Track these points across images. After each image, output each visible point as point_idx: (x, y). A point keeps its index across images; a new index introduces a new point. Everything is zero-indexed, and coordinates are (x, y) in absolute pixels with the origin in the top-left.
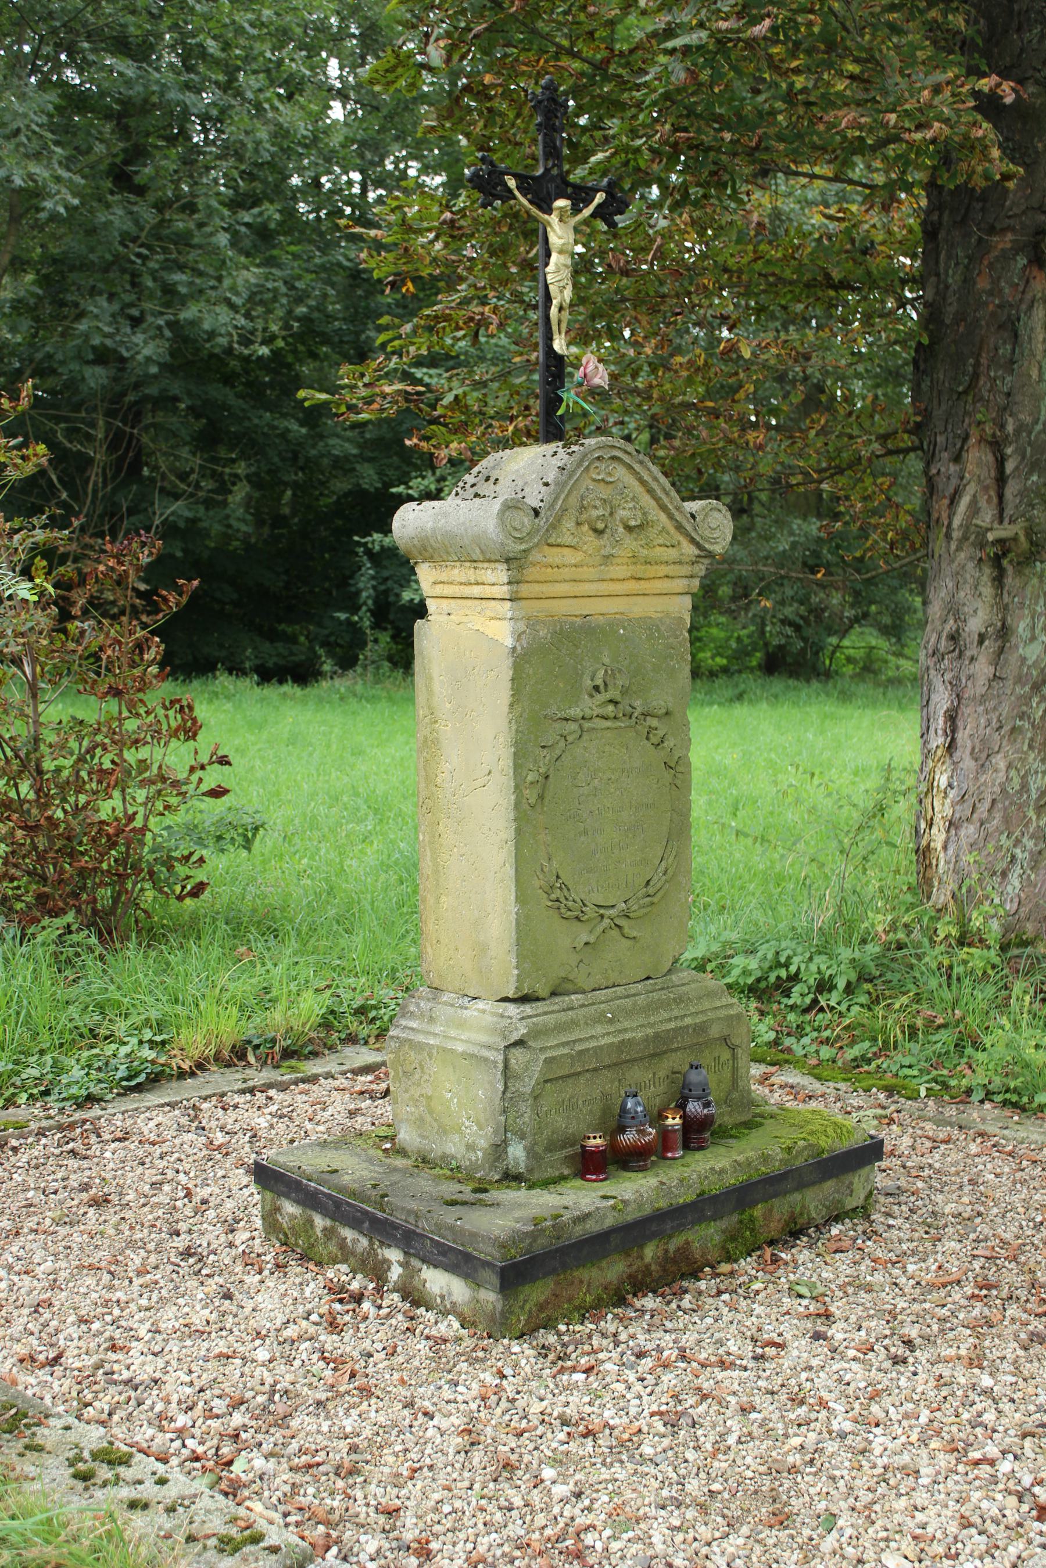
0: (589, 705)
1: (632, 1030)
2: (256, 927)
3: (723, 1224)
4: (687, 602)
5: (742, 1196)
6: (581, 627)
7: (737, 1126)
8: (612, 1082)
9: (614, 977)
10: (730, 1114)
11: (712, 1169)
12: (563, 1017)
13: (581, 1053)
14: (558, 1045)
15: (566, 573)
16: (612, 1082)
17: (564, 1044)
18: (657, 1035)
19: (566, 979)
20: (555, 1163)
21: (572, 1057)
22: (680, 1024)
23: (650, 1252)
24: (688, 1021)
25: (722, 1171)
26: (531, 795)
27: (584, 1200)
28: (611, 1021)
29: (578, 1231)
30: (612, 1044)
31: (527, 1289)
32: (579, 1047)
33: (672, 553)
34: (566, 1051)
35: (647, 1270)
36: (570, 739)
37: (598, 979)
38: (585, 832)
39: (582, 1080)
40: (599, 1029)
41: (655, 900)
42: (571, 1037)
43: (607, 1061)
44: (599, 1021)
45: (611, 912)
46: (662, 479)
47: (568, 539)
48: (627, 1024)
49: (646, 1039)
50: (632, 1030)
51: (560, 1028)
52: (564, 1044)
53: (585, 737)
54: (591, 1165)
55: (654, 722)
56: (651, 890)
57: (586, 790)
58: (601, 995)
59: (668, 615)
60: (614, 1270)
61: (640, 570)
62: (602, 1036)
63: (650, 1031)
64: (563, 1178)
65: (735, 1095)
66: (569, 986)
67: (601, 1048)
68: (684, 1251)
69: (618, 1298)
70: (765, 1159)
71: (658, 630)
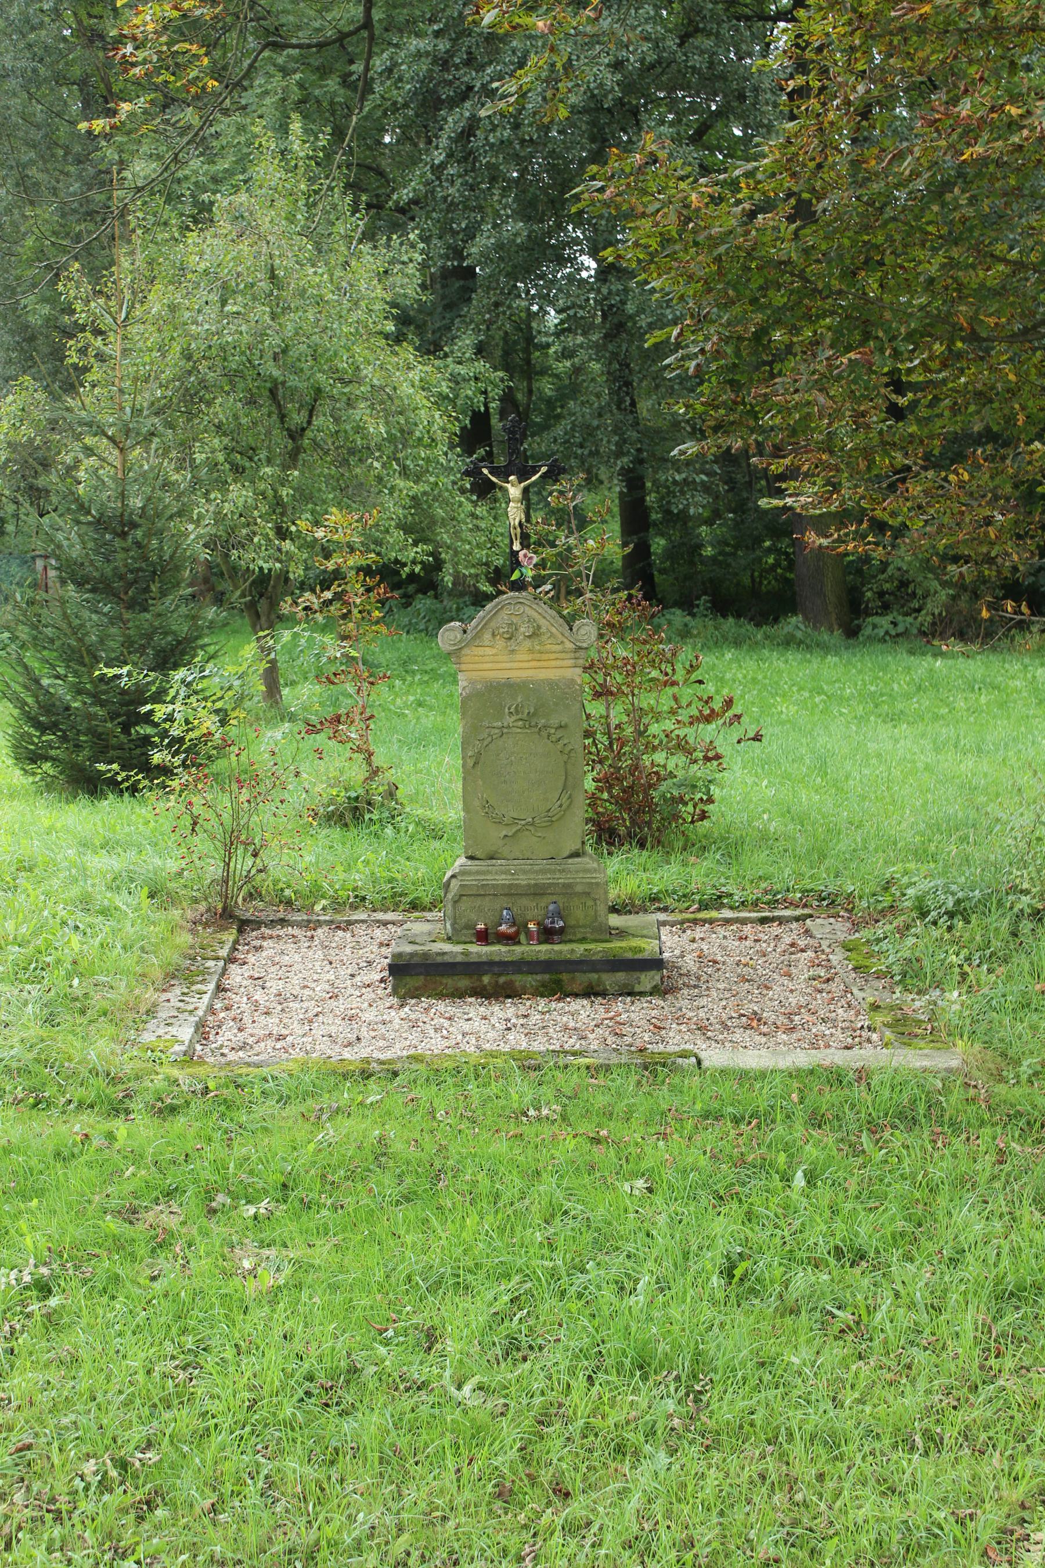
0: (509, 720)
2: (732, 849)
3: (539, 977)
5: (548, 966)
9: (528, 855)
15: (487, 659)
19: (496, 852)
23: (486, 979)
26: (470, 763)
27: (478, 951)
29: (439, 959)
31: (408, 979)
33: (559, 648)
35: (484, 987)
37: (518, 854)
39: (487, 899)
44: (502, 873)
46: (550, 611)
47: (486, 643)
49: (529, 885)
51: (478, 873)
54: (483, 937)
55: (553, 731)
58: (516, 862)
60: (464, 983)
61: (537, 656)
62: (503, 879)
68: (511, 983)
69: (459, 994)
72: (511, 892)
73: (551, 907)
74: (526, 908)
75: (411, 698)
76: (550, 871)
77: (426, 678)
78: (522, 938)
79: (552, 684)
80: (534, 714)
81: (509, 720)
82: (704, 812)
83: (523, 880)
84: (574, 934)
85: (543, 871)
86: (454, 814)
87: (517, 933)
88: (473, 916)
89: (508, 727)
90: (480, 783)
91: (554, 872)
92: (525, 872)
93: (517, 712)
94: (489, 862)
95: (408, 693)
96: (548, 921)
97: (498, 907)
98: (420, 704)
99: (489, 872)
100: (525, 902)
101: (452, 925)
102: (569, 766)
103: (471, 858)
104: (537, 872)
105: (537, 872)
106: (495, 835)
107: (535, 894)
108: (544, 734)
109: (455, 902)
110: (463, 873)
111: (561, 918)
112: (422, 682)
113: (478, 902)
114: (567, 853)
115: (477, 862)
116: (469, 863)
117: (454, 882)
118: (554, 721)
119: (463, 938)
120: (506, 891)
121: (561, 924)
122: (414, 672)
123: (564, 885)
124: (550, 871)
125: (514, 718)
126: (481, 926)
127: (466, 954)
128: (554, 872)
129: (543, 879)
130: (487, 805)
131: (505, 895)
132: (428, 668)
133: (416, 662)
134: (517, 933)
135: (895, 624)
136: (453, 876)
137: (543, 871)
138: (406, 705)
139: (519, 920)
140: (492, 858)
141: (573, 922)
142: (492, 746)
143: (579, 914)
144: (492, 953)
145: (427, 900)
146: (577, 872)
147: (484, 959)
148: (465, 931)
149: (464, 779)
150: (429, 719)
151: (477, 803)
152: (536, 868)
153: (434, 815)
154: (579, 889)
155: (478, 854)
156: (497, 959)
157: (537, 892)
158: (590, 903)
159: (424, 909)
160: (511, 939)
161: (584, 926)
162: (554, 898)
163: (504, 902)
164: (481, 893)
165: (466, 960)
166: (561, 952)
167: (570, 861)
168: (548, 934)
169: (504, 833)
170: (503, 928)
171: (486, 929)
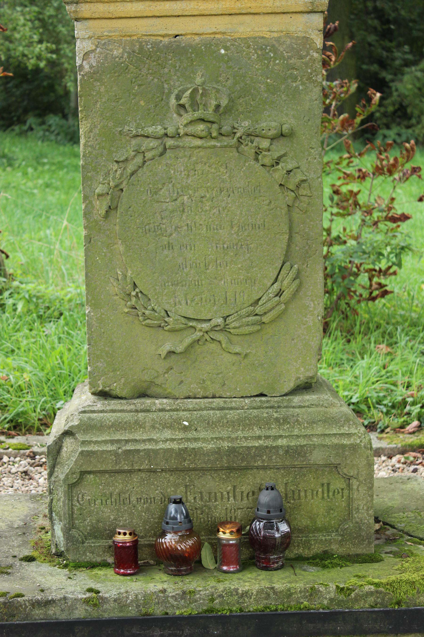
0: (178, 122)
1: (204, 440)
4: (318, 21)
6: (167, 47)
7: (341, 557)
8: (176, 486)
10: (340, 543)
11: (236, 590)
12: (128, 417)
13: (128, 452)
14: (105, 442)
16: (176, 486)
17: (112, 442)
18: (232, 451)
20: (96, 550)
21: (116, 454)
22: (269, 443)
24: (280, 442)
25: (245, 594)
28: (185, 429)
29: (38, 615)
30: (171, 450)
32: (129, 447)
34: (110, 447)
36: (149, 155)
37: (184, 390)
38: (170, 246)
39: (136, 478)
40: (167, 434)
41: (265, 319)
42: (117, 437)
43: (163, 465)
44: (171, 427)
45: (205, 326)
48: (202, 435)
49: (218, 451)
50: (204, 440)
51: (117, 426)
52: (112, 442)
53: (169, 154)
54: (129, 559)
55: (265, 144)
56: (258, 310)
57: (171, 206)
58: (191, 403)
59: (288, 35)
62: (166, 440)
63: (226, 445)
64: (105, 565)
65: (349, 525)
66: (158, 390)
67: (156, 452)
70: (313, 593)
71: (274, 49)
72: (184, 465)
73: (265, 497)
74: (213, 496)
75: (40, 181)
76: (258, 422)
77: (53, 168)
78: (207, 556)
79: (265, 49)
80: (228, 110)
81: (178, 122)
82: (381, 285)
83: (207, 441)
84: (307, 544)
85: (245, 423)
86: (74, 288)
87: (197, 549)
88: (108, 513)
89: (177, 136)
90: (120, 247)
91: (267, 423)
92: (210, 424)
93: (195, 105)
94: (139, 403)
95: (38, 177)
96: (259, 525)
97: (156, 494)
98: (48, 186)
99: (138, 425)
100: (209, 483)
101: (67, 531)
102: (296, 215)
103: (104, 395)
104: (233, 424)
105: (233, 424)
106: (149, 351)
107: (230, 469)
108: (248, 149)
109: (72, 486)
110: (87, 427)
111: (283, 519)
112: (49, 170)
113: (118, 485)
114: (290, 385)
115: (114, 404)
116: (100, 405)
117: (68, 443)
118: (269, 124)
119: (89, 557)
120: (173, 463)
121: (284, 528)
122: (44, 164)
123: (288, 450)
124: (258, 422)
125: (187, 117)
126: (123, 538)
127: (95, 599)
128: (267, 423)
129: (248, 439)
130: (133, 291)
131: (172, 471)
132: (56, 161)
133: (46, 157)
134: (197, 549)
135: (399, 135)
136: (68, 433)
137: (245, 423)
138: (36, 187)
139: (199, 519)
140: (143, 395)
141: (305, 522)
142: (144, 175)
143: (316, 506)
144: (147, 598)
145: (34, 418)
146: (312, 422)
147: (132, 612)
148: (91, 543)
149: (88, 239)
150: (53, 197)
151: (113, 288)
152: (232, 415)
153: (50, 290)
154: (317, 457)
155: (117, 388)
156: (158, 611)
157: (235, 463)
158: (338, 484)
159: (29, 430)
160: (184, 563)
161: (326, 529)
162: (267, 477)
163: (173, 486)
164: (125, 466)
165: (95, 614)
166: (289, 594)
167: (296, 399)
168: (259, 551)
169: (167, 347)
170: (170, 540)
171: (135, 543)
